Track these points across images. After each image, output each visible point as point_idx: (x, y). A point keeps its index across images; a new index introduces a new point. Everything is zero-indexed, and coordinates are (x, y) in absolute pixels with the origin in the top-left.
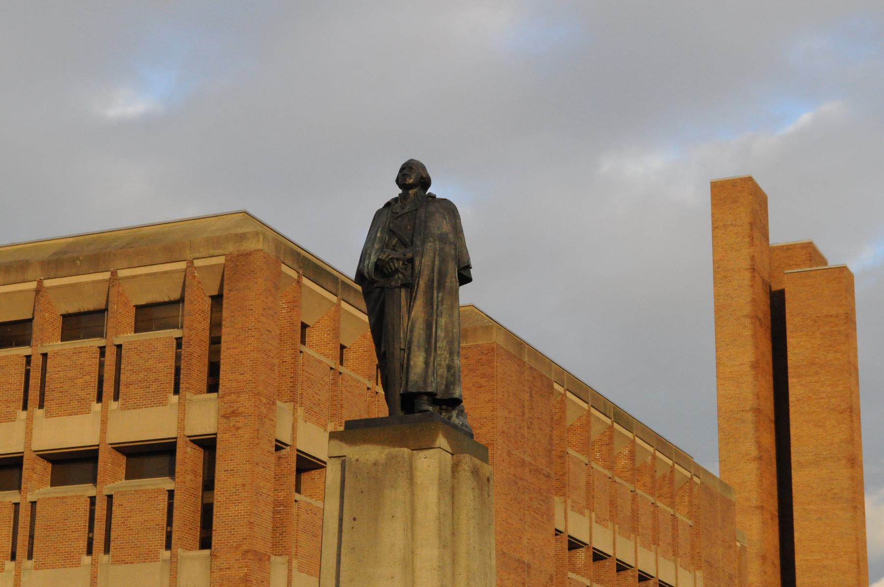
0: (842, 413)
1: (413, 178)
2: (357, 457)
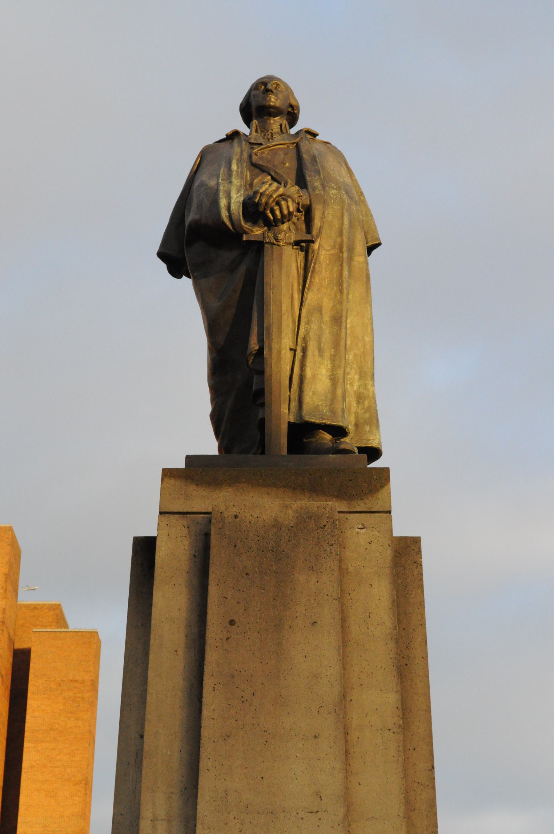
0: (76, 784)
2: (235, 510)
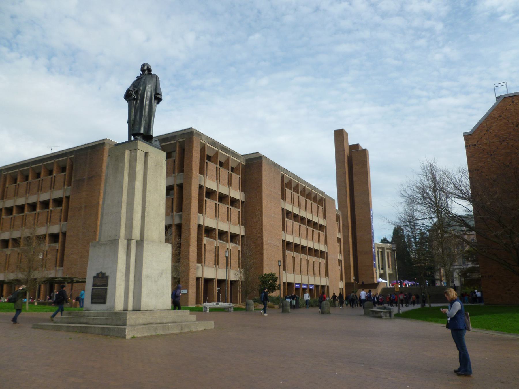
1: (146, 70)
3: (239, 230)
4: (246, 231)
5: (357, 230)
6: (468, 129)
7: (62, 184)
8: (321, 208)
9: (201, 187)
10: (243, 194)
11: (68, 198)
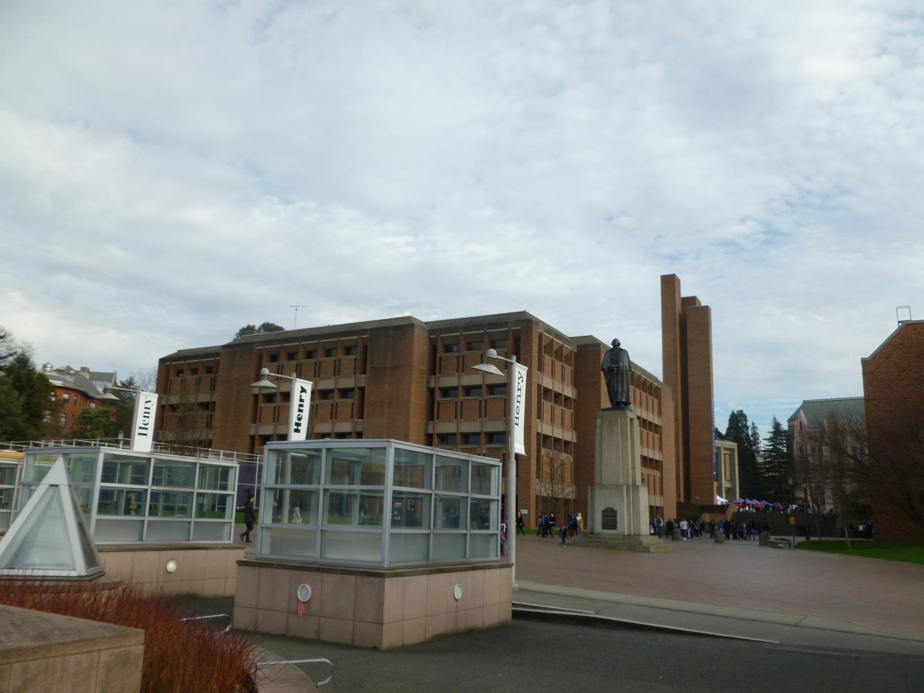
3: (569, 436)
4: (578, 437)
5: (691, 425)
6: (867, 355)
7: (352, 371)
8: (656, 401)
9: (539, 386)
10: (575, 391)
11: (362, 390)
